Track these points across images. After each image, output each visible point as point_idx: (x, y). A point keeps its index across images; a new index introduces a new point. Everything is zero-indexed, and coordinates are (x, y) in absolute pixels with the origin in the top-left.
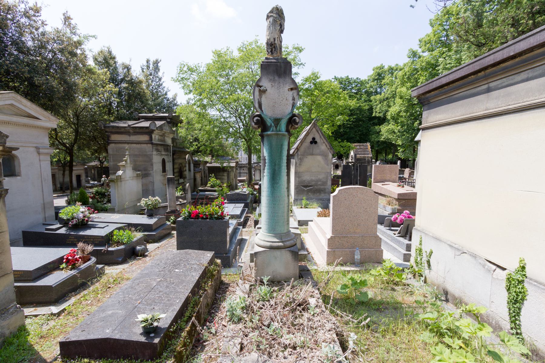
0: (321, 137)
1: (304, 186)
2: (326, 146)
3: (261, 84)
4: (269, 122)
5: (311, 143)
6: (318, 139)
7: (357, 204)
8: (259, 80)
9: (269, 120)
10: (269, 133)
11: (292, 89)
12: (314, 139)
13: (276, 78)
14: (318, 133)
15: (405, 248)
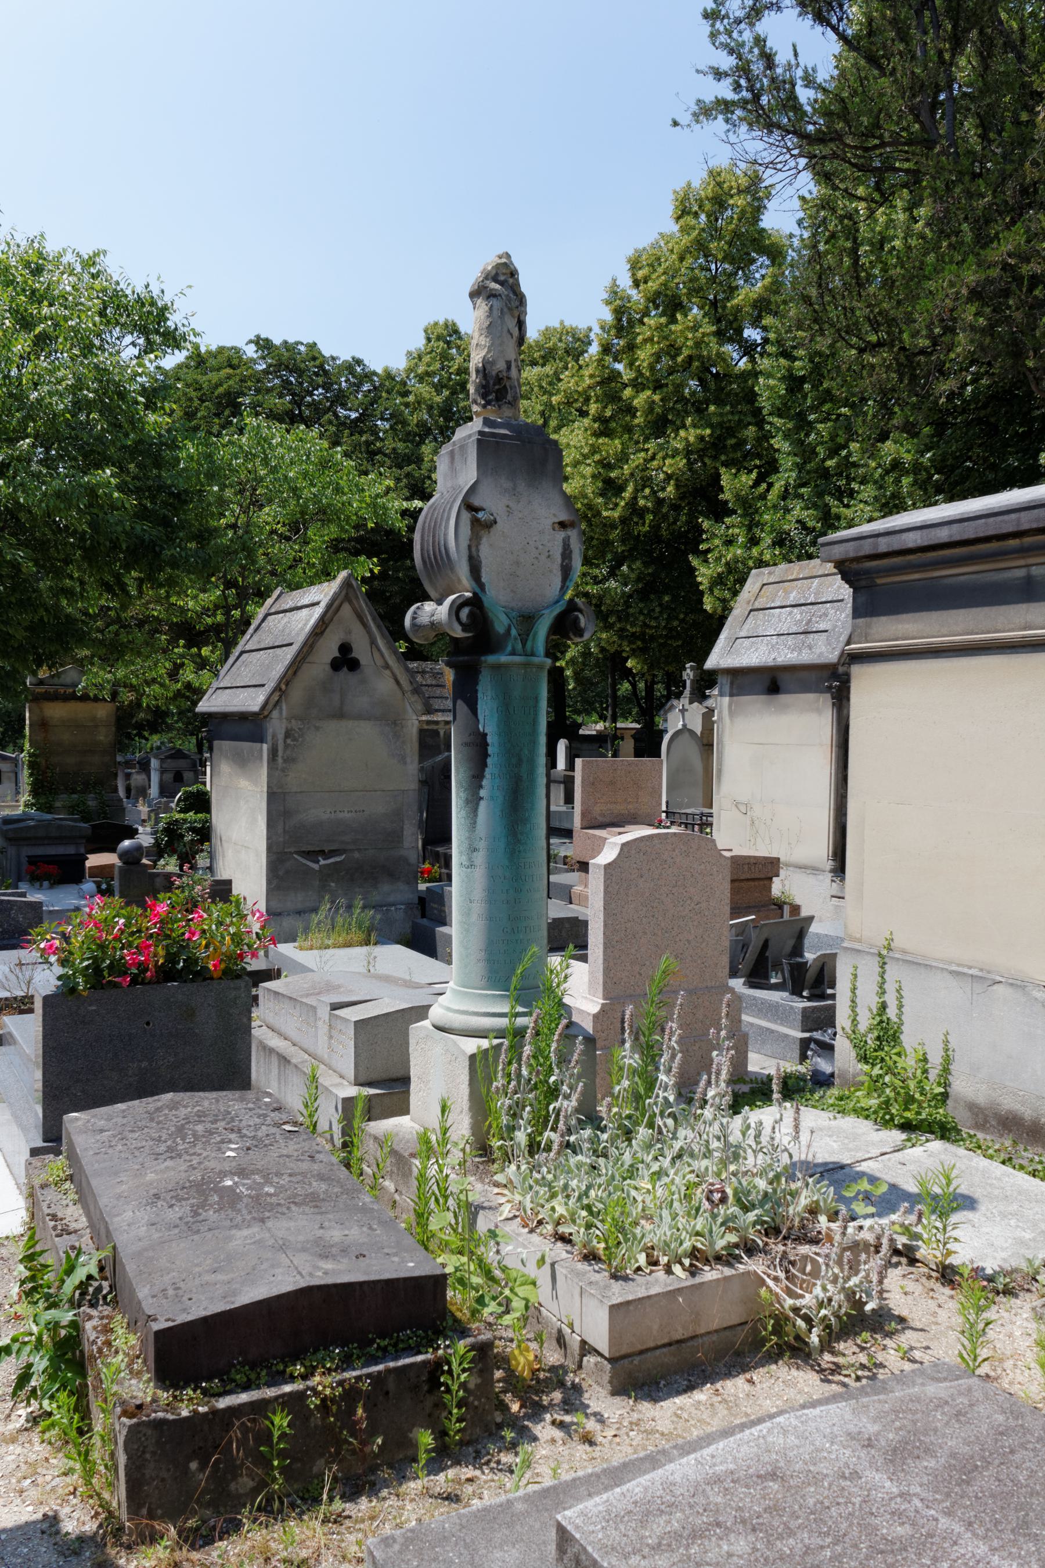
0: (373, 642)
1: (309, 855)
2: (398, 682)
3: (476, 502)
4: (500, 622)
5: (336, 665)
6: (361, 651)
7: (674, 890)
8: (473, 489)
9: (503, 618)
10: (504, 659)
11: (563, 525)
12: (345, 648)
13: (522, 486)
14: (365, 625)
15: (798, 1023)
